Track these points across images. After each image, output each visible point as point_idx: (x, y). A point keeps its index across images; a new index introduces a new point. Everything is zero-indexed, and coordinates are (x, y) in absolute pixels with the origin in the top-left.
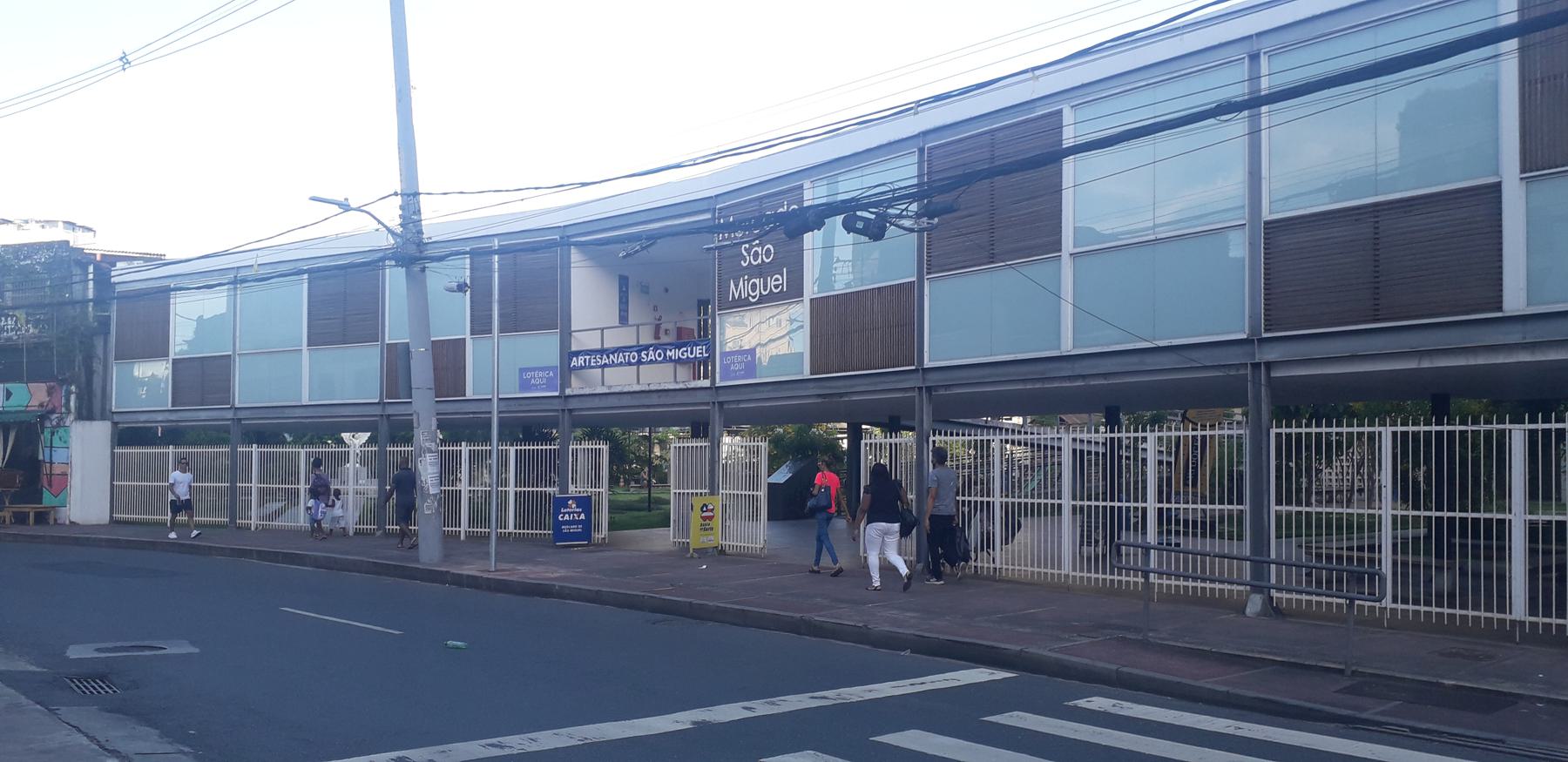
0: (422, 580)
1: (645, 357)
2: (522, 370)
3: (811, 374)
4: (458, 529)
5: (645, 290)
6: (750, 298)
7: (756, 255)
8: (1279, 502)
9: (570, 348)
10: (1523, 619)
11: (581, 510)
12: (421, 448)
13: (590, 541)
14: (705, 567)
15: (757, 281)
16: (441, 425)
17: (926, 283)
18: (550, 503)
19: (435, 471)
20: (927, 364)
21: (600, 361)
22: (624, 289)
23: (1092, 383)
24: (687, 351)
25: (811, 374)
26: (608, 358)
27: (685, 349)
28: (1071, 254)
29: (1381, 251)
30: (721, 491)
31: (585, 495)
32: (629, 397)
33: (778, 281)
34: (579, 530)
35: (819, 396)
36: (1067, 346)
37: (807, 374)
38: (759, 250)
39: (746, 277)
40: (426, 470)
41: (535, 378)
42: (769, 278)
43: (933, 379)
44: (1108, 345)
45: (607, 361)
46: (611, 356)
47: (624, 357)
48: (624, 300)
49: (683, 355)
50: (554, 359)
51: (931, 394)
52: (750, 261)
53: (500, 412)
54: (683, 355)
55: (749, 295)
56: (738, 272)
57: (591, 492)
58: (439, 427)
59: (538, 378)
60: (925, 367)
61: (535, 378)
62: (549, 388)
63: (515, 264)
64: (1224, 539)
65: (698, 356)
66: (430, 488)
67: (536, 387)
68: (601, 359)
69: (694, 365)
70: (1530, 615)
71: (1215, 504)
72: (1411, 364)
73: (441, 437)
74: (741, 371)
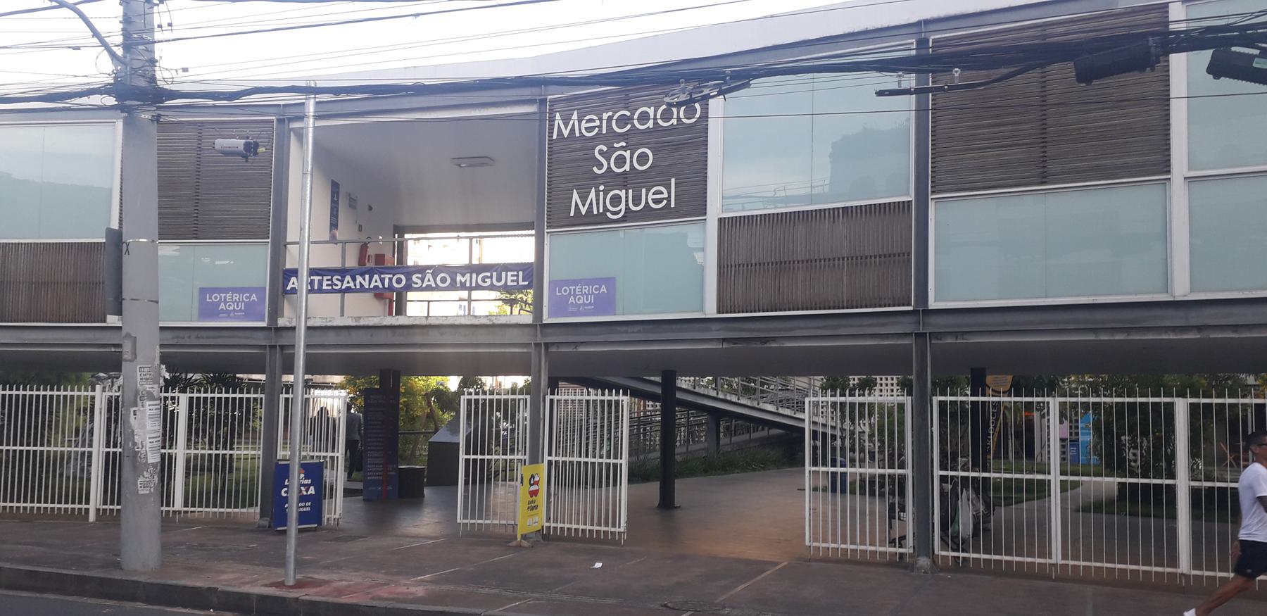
0: (149, 600)
1: (419, 281)
2: (203, 291)
3: (719, 312)
4: (84, 506)
5: (353, 204)
6: (608, 214)
7: (621, 161)
8: (467, 453)
9: (285, 264)
10: (1188, 573)
11: (310, 481)
12: (137, 392)
13: (319, 521)
14: (598, 565)
15: (622, 194)
16: (164, 359)
17: (932, 206)
18: (7, 462)
19: (157, 428)
20: (933, 304)
21: (339, 283)
22: (335, 199)
23: (1212, 336)
24: (491, 277)
25: (719, 312)
26: (354, 280)
27: (488, 274)
28: (1185, 178)
29: (737, 263)
30: (547, 458)
31: (315, 461)
32: (389, 332)
33: (666, 193)
34: (308, 509)
35: (724, 340)
36: (1181, 289)
37: (711, 310)
38: (627, 154)
39: (602, 188)
40: (143, 426)
41: (225, 303)
42: (644, 191)
43: (938, 323)
44: (1251, 290)
45: (352, 284)
46: (359, 279)
47: (382, 281)
48: (335, 213)
49: (484, 281)
50: (261, 276)
51: (548, 349)
52: (609, 167)
53: (308, 346)
54: (484, 281)
55: (606, 209)
56: (586, 182)
57: (325, 457)
58: (162, 362)
59: (232, 302)
60: (544, 322)
61: (225, 303)
62: (250, 312)
63: (200, 149)
64: (875, 495)
65: (509, 283)
66: (149, 454)
67: (228, 314)
68: (342, 281)
69: (391, 301)
70: (1193, 569)
71: (477, 454)
72: (1091, 337)
73: (167, 376)
74: (588, 305)
